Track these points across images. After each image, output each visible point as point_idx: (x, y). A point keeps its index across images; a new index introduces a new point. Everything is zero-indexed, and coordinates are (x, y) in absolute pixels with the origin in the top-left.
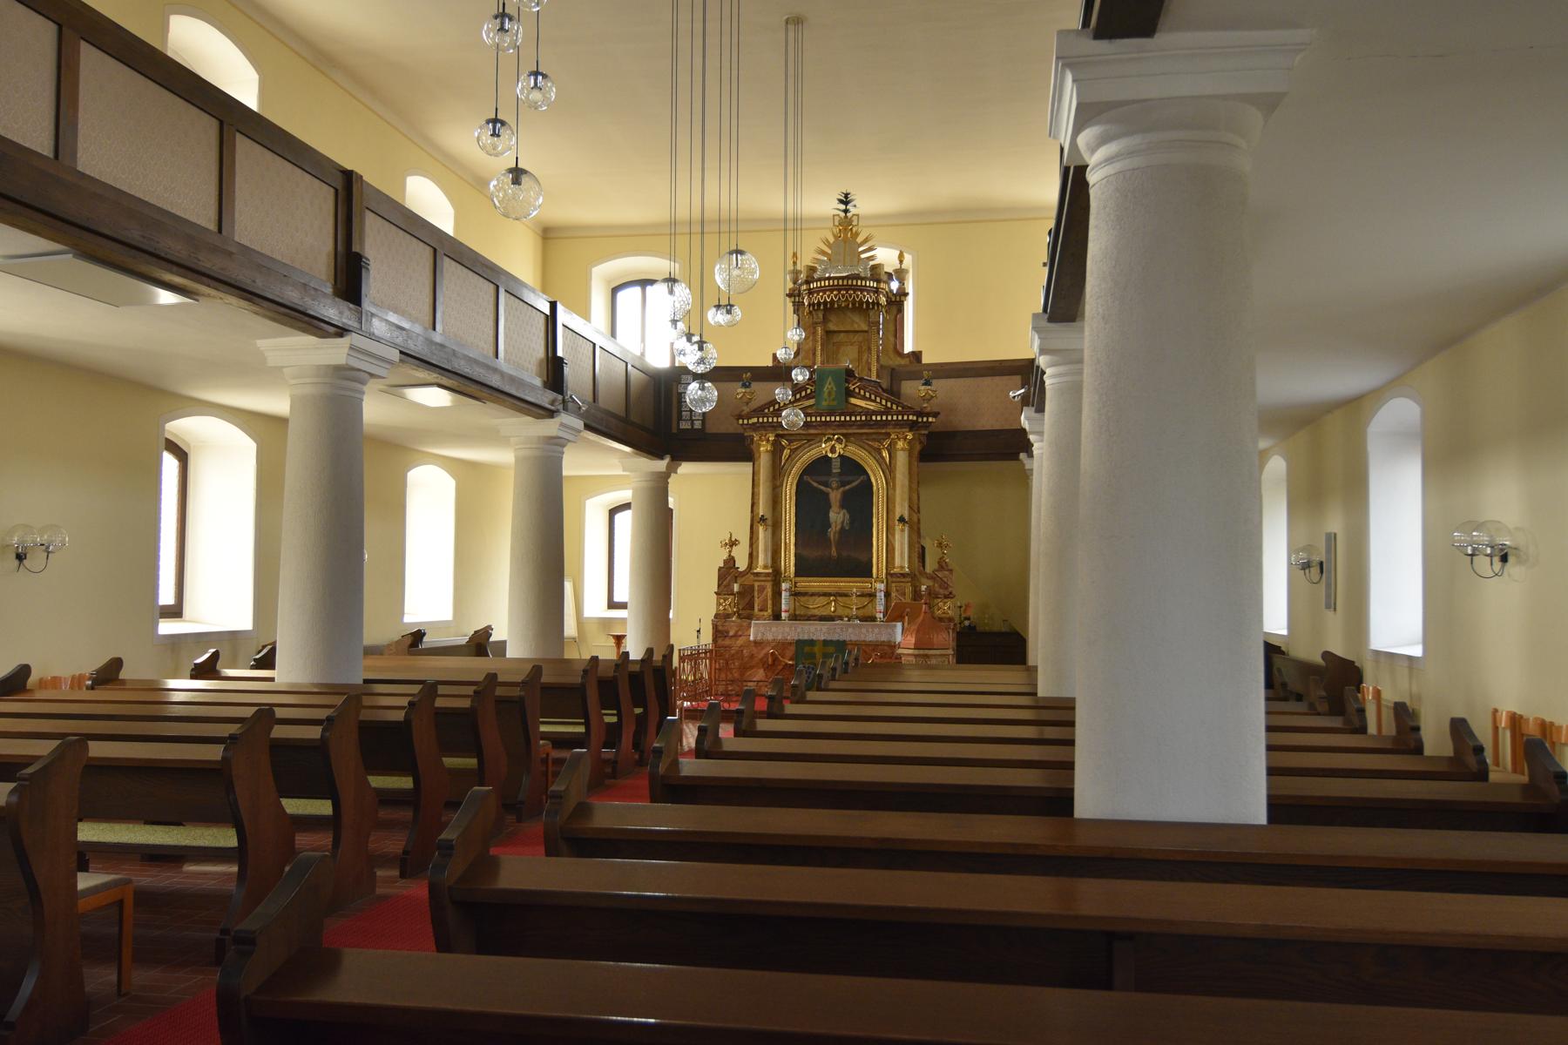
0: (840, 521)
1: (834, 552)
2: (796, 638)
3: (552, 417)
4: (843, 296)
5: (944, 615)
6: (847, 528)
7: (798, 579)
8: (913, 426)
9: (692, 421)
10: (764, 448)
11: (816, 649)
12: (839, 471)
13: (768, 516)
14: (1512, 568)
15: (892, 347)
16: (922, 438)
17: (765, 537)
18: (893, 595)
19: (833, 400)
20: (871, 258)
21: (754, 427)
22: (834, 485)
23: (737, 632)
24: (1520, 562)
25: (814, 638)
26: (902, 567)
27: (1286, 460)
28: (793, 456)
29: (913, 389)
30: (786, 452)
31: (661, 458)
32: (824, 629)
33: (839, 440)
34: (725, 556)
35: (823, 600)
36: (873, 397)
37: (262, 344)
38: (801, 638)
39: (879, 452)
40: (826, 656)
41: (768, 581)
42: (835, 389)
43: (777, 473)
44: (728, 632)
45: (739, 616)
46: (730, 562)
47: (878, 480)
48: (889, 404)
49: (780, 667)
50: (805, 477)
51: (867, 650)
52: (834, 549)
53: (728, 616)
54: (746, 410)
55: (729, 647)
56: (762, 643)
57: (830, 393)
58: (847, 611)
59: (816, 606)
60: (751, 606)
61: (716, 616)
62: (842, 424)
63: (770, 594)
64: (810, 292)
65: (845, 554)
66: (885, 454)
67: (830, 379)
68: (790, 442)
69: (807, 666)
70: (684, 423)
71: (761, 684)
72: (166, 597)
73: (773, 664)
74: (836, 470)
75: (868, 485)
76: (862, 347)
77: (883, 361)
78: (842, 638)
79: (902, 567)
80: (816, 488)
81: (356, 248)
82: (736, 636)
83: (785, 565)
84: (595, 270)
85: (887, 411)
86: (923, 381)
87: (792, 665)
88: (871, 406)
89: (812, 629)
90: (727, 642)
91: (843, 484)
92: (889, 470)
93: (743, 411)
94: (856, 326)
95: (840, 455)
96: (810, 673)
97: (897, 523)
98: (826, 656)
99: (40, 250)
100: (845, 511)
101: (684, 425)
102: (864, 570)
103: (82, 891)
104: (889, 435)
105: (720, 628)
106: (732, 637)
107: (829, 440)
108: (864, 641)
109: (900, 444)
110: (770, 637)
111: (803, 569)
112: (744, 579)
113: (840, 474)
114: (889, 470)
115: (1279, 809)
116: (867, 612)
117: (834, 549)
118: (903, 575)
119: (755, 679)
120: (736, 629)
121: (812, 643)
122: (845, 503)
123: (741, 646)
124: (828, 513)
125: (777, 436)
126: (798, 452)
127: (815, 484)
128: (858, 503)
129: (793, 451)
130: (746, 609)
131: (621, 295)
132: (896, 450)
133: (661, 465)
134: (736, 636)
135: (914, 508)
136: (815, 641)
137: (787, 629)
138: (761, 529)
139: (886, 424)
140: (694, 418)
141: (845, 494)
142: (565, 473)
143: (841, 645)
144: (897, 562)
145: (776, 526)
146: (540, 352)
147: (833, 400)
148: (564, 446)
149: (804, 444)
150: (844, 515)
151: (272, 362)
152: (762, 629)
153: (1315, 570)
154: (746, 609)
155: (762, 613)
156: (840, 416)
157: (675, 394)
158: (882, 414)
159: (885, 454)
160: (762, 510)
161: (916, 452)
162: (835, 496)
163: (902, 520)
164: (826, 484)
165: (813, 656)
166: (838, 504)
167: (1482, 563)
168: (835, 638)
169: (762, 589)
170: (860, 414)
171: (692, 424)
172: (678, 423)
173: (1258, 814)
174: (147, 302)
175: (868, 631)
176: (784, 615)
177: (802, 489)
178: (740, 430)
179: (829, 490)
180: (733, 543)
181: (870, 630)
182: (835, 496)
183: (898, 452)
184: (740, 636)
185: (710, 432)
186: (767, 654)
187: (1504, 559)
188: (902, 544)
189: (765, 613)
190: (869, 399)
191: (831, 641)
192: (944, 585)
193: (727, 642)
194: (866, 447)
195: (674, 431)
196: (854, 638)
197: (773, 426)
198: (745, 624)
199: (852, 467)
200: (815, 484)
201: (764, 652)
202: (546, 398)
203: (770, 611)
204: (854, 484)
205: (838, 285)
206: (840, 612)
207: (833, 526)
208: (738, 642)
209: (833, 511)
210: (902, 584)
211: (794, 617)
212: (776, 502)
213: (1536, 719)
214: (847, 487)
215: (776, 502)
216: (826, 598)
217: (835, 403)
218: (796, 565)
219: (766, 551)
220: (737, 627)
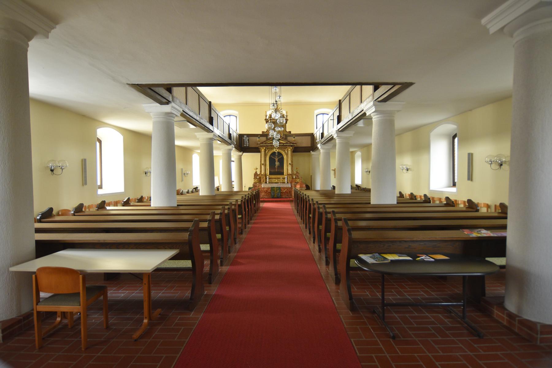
1: (276, 170)
3: (230, 145)
8: (292, 146)
9: (247, 145)
10: (263, 150)
11: (275, 189)
14: (409, 171)
18: (288, 178)
20: (282, 113)
21: (261, 146)
22: (276, 157)
24: (411, 170)
26: (290, 173)
27: (361, 152)
29: (290, 139)
30: (267, 151)
31: (241, 152)
33: (277, 149)
34: (255, 171)
35: (275, 179)
37: (196, 134)
39: (285, 151)
43: (265, 155)
45: (259, 183)
46: (256, 172)
47: (285, 157)
53: (256, 183)
54: (259, 143)
58: (279, 182)
59: (273, 180)
60: (260, 181)
61: (254, 183)
63: (265, 179)
64: (271, 120)
65: (279, 170)
66: (286, 151)
68: (268, 149)
72: (99, 184)
73: (267, 192)
74: (277, 154)
75: (283, 158)
79: (290, 173)
81: (212, 116)
82: (258, 187)
85: (287, 143)
86: (293, 137)
88: (284, 142)
89: (274, 185)
91: (278, 157)
92: (287, 154)
98: (277, 190)
99: (181, 120)
101: (245, 146)
102: (282, 174)
103: (240, 215)
104: (287, 148)
107: (275, 149)
109: (289, 149)
110: (266, 187)
111: (271, 173)
113: (278, 155)
114: (287, 154)
115: (398, 203)
116: (283, 181)
118: (290, 174)
121: (274, 188)
122: (279, 161)
125: (266, 148)
127: (273, 157)
128: (281, 160)
129: (268, 151)
130: (260, 181)
132: (288, 151)
133: (241, 153)
135: (292, 162)
138: (263, 166)
139: (287, 146)
141: (279, 159)
142: (214, 155)
143: (280, 188)
144: (289, 172)
145: (265, 165)
146: (228, 133)
148: (231, 150)
151: (198, 137)
152: (264, 185)
153: (369, 172)
154: (260, 181)
157: (243, 139)
158: (286, 144)
159: (286, 151)
160: (263, 162)
161: (292, 151)
162: (277, 160)
163: (290, 164)
164: (275, 157)
165: (274, 190)
167: (405, 171)
169: (263, 178)
170: (282, 144)
173: (396, 203)
174: (188, 126)
176: (267, 182)
177: (270, 158)
178: (258, 147)
180: (257, 169)
182: (277, 160)
183: (508, 159)
187: (408, 170)
188: (290, 168)
190: (283, 141)
192: (298, 176)
193: (256, 188)
195: (243, 146)
199: (280, 154)
200: (273, 157)
202: (229, 141)
206: (278, 182)
211: (269, 183)
212: (265, 161)
213: (419, 195)
215: (265, 161)
218: (269, 173)
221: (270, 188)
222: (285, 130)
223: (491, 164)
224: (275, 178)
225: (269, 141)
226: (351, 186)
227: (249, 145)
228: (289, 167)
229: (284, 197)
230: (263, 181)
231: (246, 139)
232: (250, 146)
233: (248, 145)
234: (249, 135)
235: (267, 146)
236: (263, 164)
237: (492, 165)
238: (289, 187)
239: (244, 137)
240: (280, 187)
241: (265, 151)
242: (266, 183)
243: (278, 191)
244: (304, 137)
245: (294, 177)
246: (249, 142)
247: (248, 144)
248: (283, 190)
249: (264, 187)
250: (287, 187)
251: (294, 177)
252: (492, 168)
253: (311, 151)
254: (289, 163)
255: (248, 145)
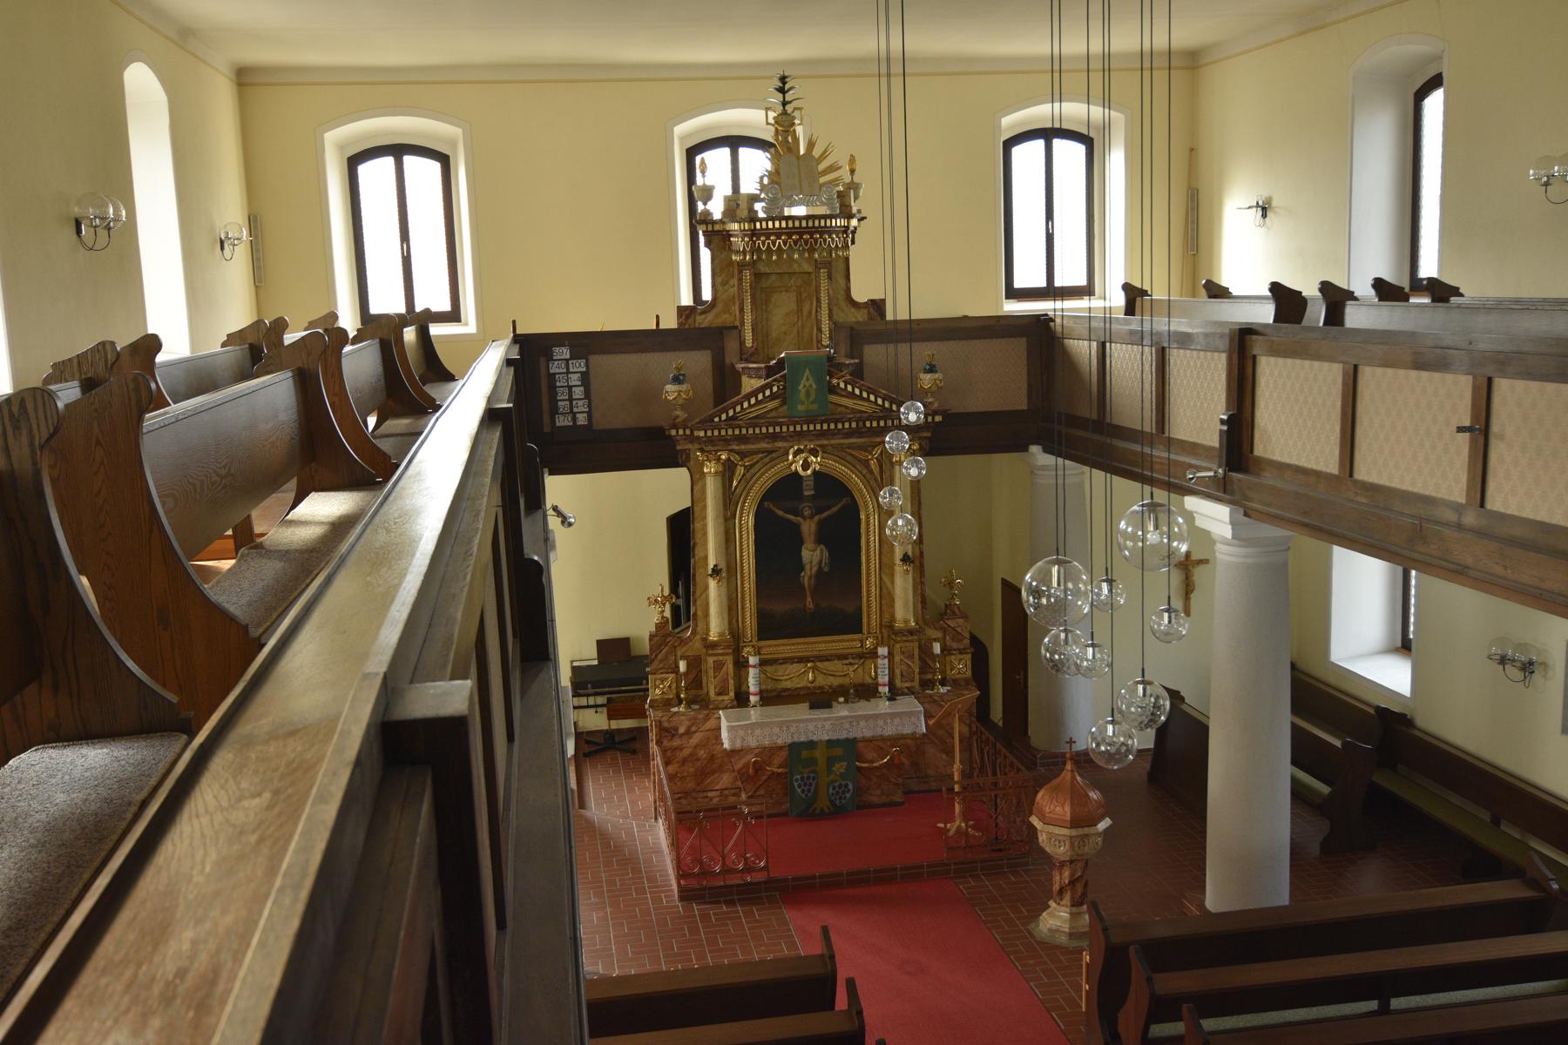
0: (815, 562)
2: (789, 741)
4: (806, 242)
5: (959, 676)
6: (826, 569)
7: (762, 643)
9: (574, 414)
12: (813, 492)
13: (722, 565)
15: (842, 293)
16: (923, 443)
17: (719, 595)
18: (897, 659)
19: (812, 403)
23: (690, 727)
25: (815, 738)
26: (906, 621)
28: (748, 475)
32: (828, 725)
36: (865, 395)
38: (796, 740)
40: (831, 761)
41: (727, 654)
42: (814, 386)
44: (676, 729)
48: (887, 405)
49: (765, 778)
50: (766, 503)
51: (883, 746)
52: (809, 599)
55: (681, 749)
56: (742, 750)
57: (808, 394)
62: (822, 434)
63: (731, 671)
66: (873, 464)
67: (807, 373)
69: (806, 776)
70: (562, 418)
71: (727, 792)
76: (801, 294)
77: (840, 317)
78: (851, 735)
79: (906, 621)
80: (782, 518)
82: (688, 733)
83: (741, 556)
84: (326, 135)
87: (787, 773)
90: (676, 742)
91: (819, 511)
93: (677, 417)
94: (796, 266)
95: (815, 472)
96: (811, 785)
97: (898, 561)
98: (831, 761)
100: (822, 546)
101: (563, 421)
102: (852, 624)
105: (666, 725)
106: (683, 734)
108: (881, 736)
110: (753, 743)
111: (769, 627)
112: (684, 649)
117: (809, 599)
118: (911, 632)
119: (717, 788)
120: (687, 723)
121: (811, 745)
123: (695, 747)
124: (800, 551)
126: (752, 471)
127: (780, 513)
129: (747, 469)
131: (364, 170)
134: (688, 733)
136: (816, 743)
137: (776, 730)
140: (575, 410)
141: (821, 524)
143: (850, 747)
147: (812, 403)
149: (762, 458)
150: (822, 551)
152: (741, 733)
155: (720, 698)
156: (828, 422)
162: (808, 528)
164: (796, 513)
165: (812, 761)
166: (812, 538)
168: (843, 735)
169: (719, 666)
171: (574, 419)
172: (553, 422)
175: (886, 723)
176: (753, 699)
177: (763, 519)
179: (800, 519)
181: (889, 721)
182: (808, 528)
184: (695, 732)
185: (601, 427)
186: (746, 765)
189: (726, 698)
190: (860, 397)
191: (838, 740)
193: (676, 742)
194: (849, 458)
195: (547, 429)
196: (868, 734)
197: (724, 440)
198: (701, 716)
200: (780, 513)
201: (744, 761)
203: (732, 694)
204: (834, 509)
205: (800, 227)
207: (808, 567)
208: (692, 741)
209: (807, 549)
210: (908, 644)
211: (768, 698)
214: (825, 514)
216: (802, 665)
217: (815, 407)
219: (721, 614)
220: (690, 720)
221: (781, 748)
222: (841, 296)
223: (1546, 184)
224: (802, 660)
225: (758, 402)
226: (1293, 667)
227: (589, 414)
228: (899, 580)
229: (875, 800)
230: (722, 692)
231: (565, 369)
232: (602, 423)
233: (582, 420)
234: (586, 344)
235: (742, 439)
236: (716, 572)
237: (1549, 187)
238: (913, 736)
239: (550, 358)
240: (850, 743)
241: (728, 471)
242: (742, 700)
243: (840, 767)
244: (979, 345)
245: (937, 648)
246: (587, 395)
247: (581, 406)
248: (871, 755)
249: (738, 745)
250: (903, 737)
251: (937, 648)
252: (1549, 200)
253: (1035, 449)
254: (898, 554)
255: (582, 420)
